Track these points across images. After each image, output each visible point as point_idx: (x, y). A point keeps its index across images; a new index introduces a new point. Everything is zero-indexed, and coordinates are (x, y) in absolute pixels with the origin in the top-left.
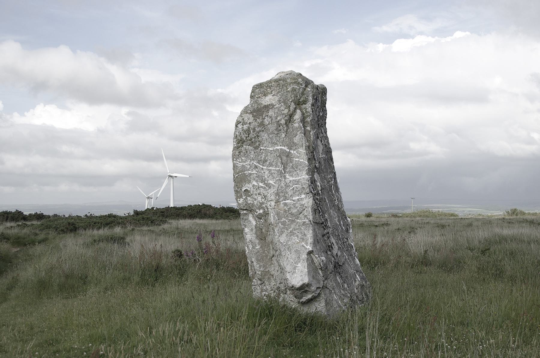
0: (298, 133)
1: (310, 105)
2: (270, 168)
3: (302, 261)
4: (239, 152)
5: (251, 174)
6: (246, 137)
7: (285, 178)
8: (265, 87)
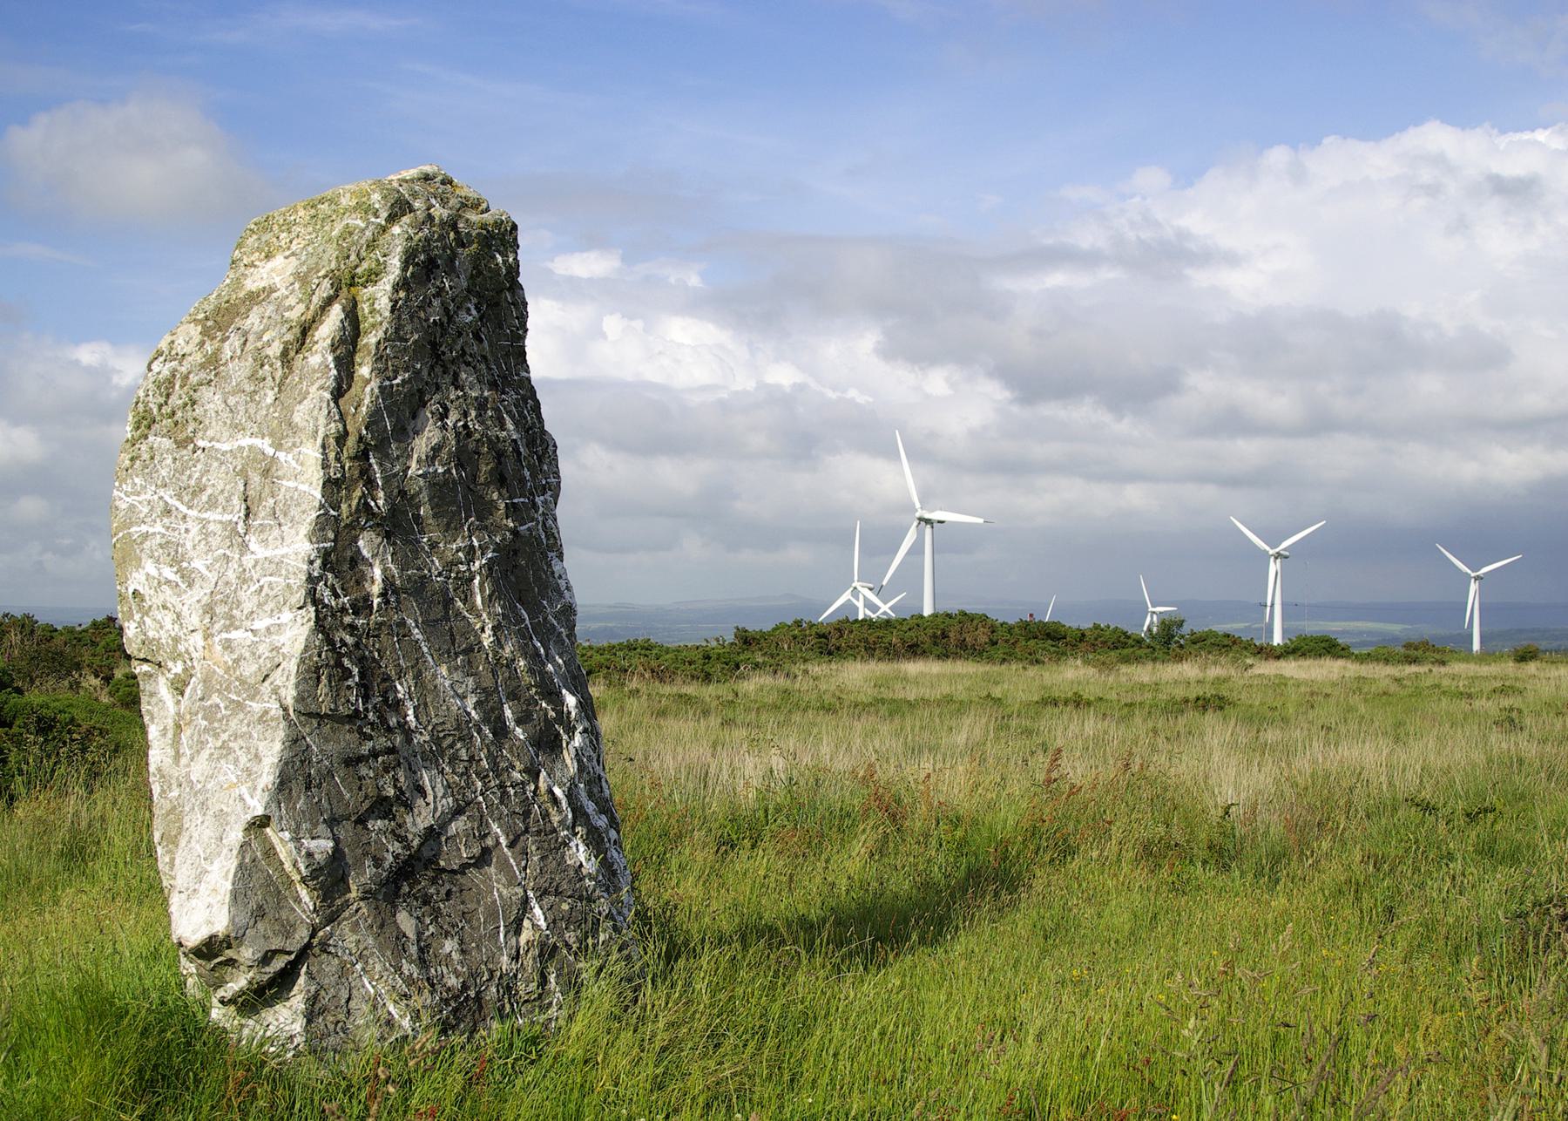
0: (313, 389)
1: (389, 288)
2: (205, 515)
3: (225, 851)
4: (132, 459)
5: (146, 536)
6: (160, 406)
7: (244, 547)
8: (276, 227)
